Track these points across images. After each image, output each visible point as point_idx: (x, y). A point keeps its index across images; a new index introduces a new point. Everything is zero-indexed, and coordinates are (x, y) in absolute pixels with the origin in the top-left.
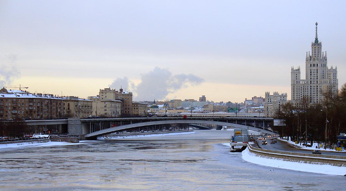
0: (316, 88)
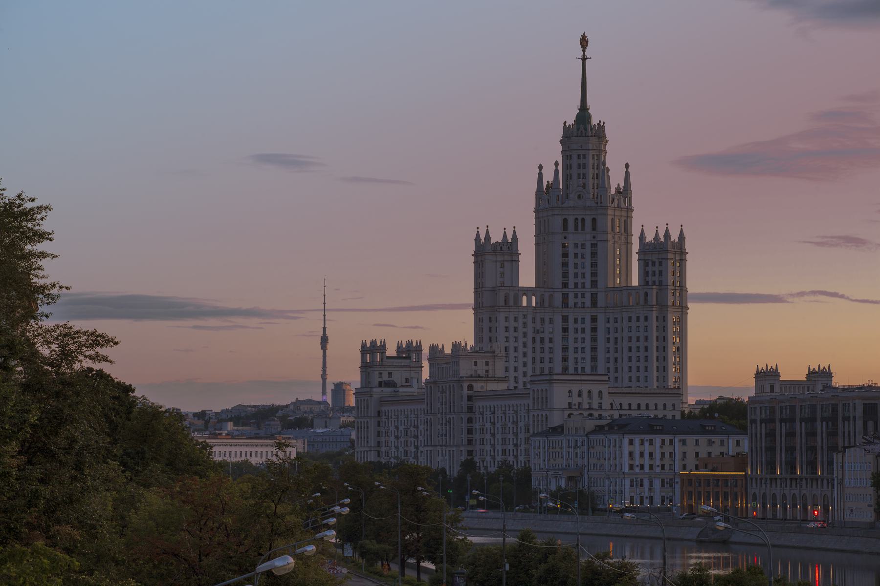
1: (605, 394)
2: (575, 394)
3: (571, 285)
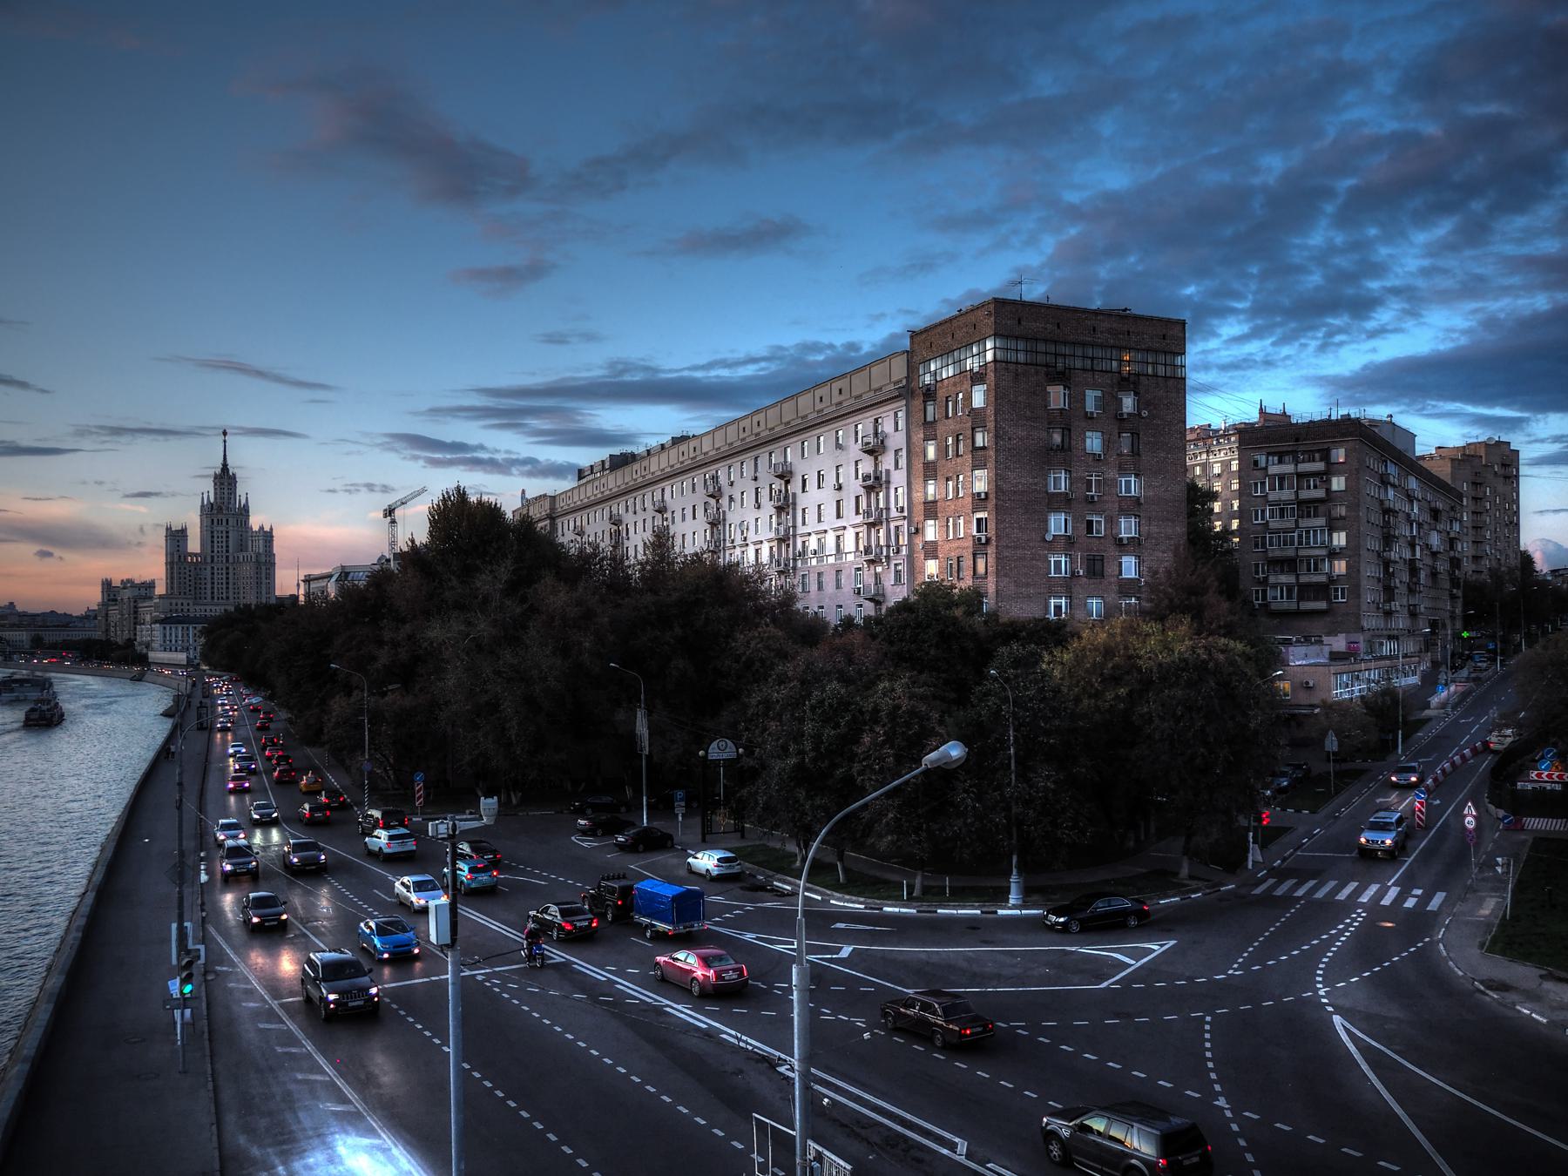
0: (224, 572)
1: (191, 604)
2: (174, 604)
3: (216, 551)
